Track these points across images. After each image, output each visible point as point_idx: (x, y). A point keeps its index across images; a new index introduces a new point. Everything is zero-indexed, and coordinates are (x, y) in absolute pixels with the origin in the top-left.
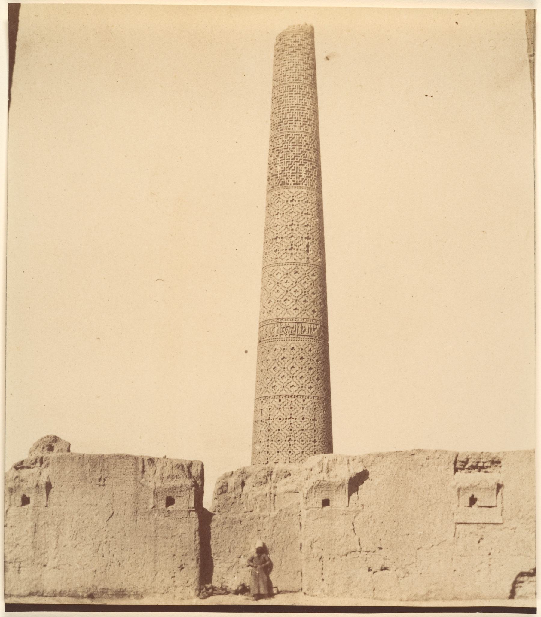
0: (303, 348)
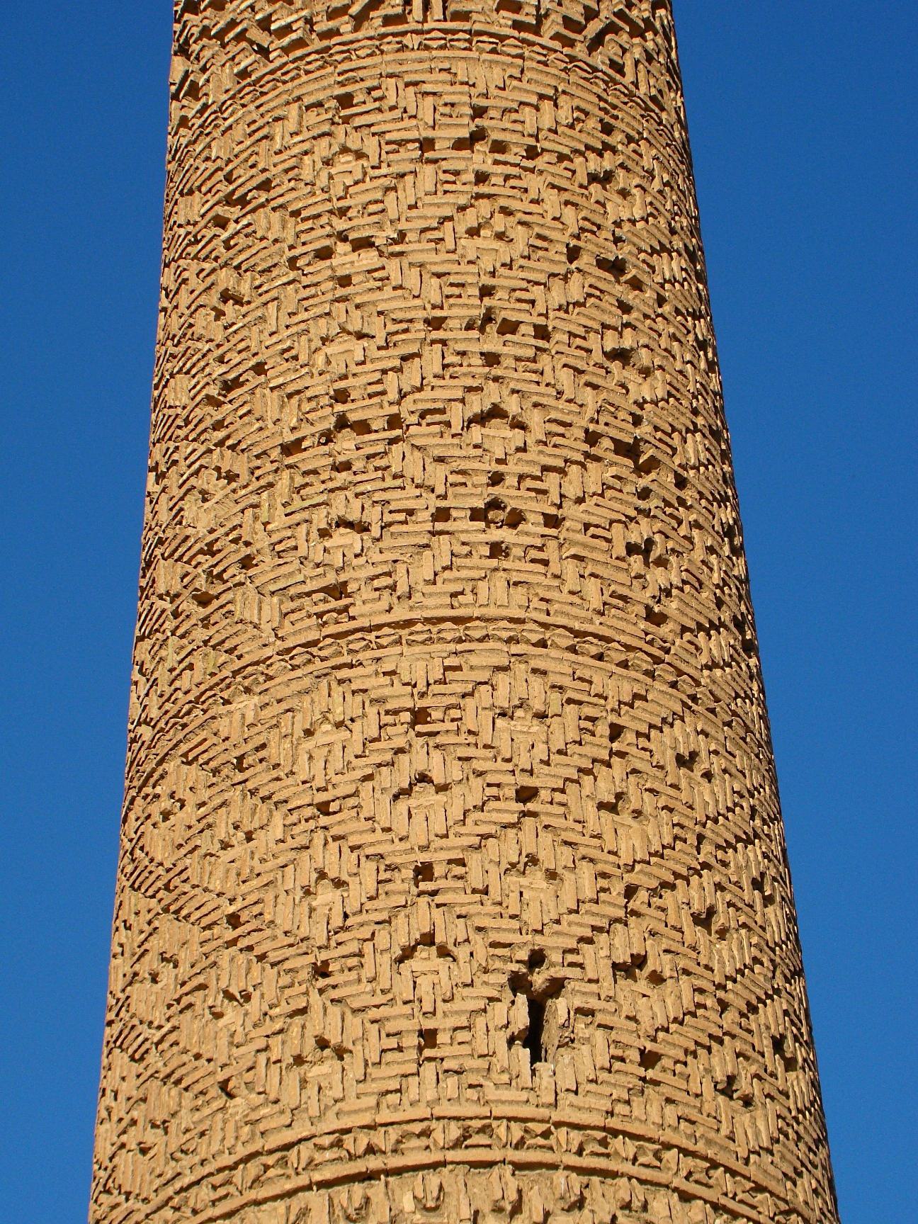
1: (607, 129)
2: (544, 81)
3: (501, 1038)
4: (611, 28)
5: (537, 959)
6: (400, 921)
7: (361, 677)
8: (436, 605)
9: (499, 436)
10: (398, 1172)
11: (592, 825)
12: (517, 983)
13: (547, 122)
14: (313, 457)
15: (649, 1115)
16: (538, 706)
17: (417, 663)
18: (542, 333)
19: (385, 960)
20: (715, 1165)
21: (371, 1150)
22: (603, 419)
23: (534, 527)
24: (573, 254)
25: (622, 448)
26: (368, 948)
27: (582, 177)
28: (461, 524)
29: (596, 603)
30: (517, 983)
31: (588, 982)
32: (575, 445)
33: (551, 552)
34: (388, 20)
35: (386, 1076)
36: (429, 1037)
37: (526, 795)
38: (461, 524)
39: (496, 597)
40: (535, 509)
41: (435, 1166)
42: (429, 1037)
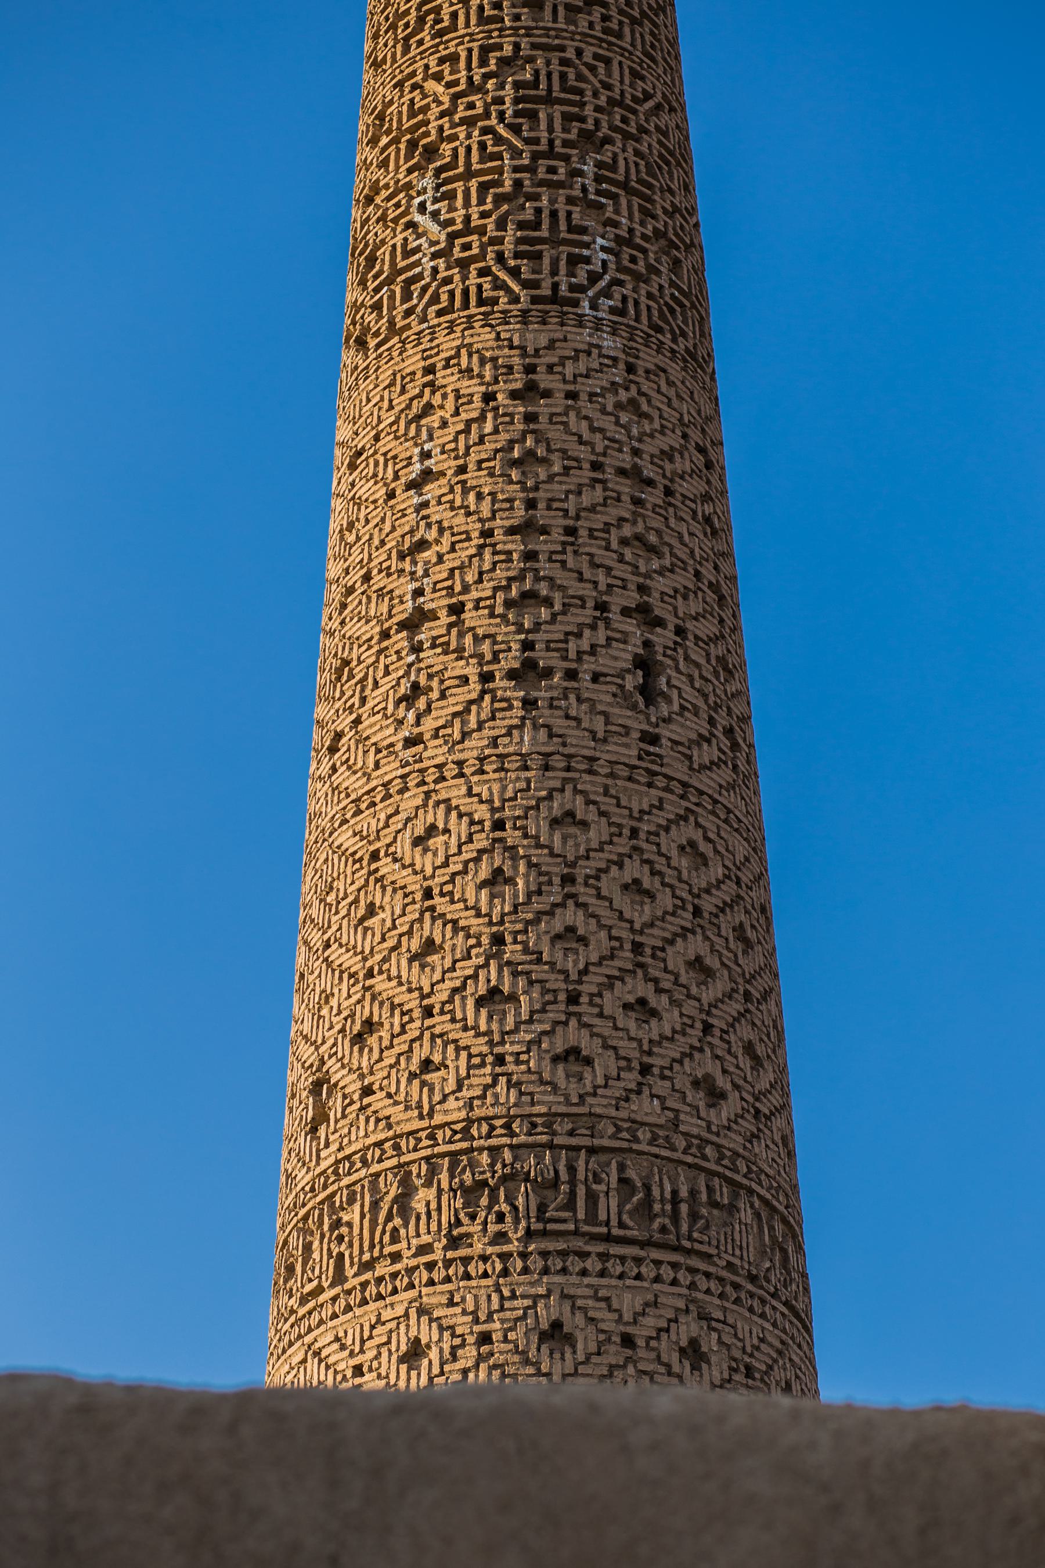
0: (639, 1334)
34: (440, 313)
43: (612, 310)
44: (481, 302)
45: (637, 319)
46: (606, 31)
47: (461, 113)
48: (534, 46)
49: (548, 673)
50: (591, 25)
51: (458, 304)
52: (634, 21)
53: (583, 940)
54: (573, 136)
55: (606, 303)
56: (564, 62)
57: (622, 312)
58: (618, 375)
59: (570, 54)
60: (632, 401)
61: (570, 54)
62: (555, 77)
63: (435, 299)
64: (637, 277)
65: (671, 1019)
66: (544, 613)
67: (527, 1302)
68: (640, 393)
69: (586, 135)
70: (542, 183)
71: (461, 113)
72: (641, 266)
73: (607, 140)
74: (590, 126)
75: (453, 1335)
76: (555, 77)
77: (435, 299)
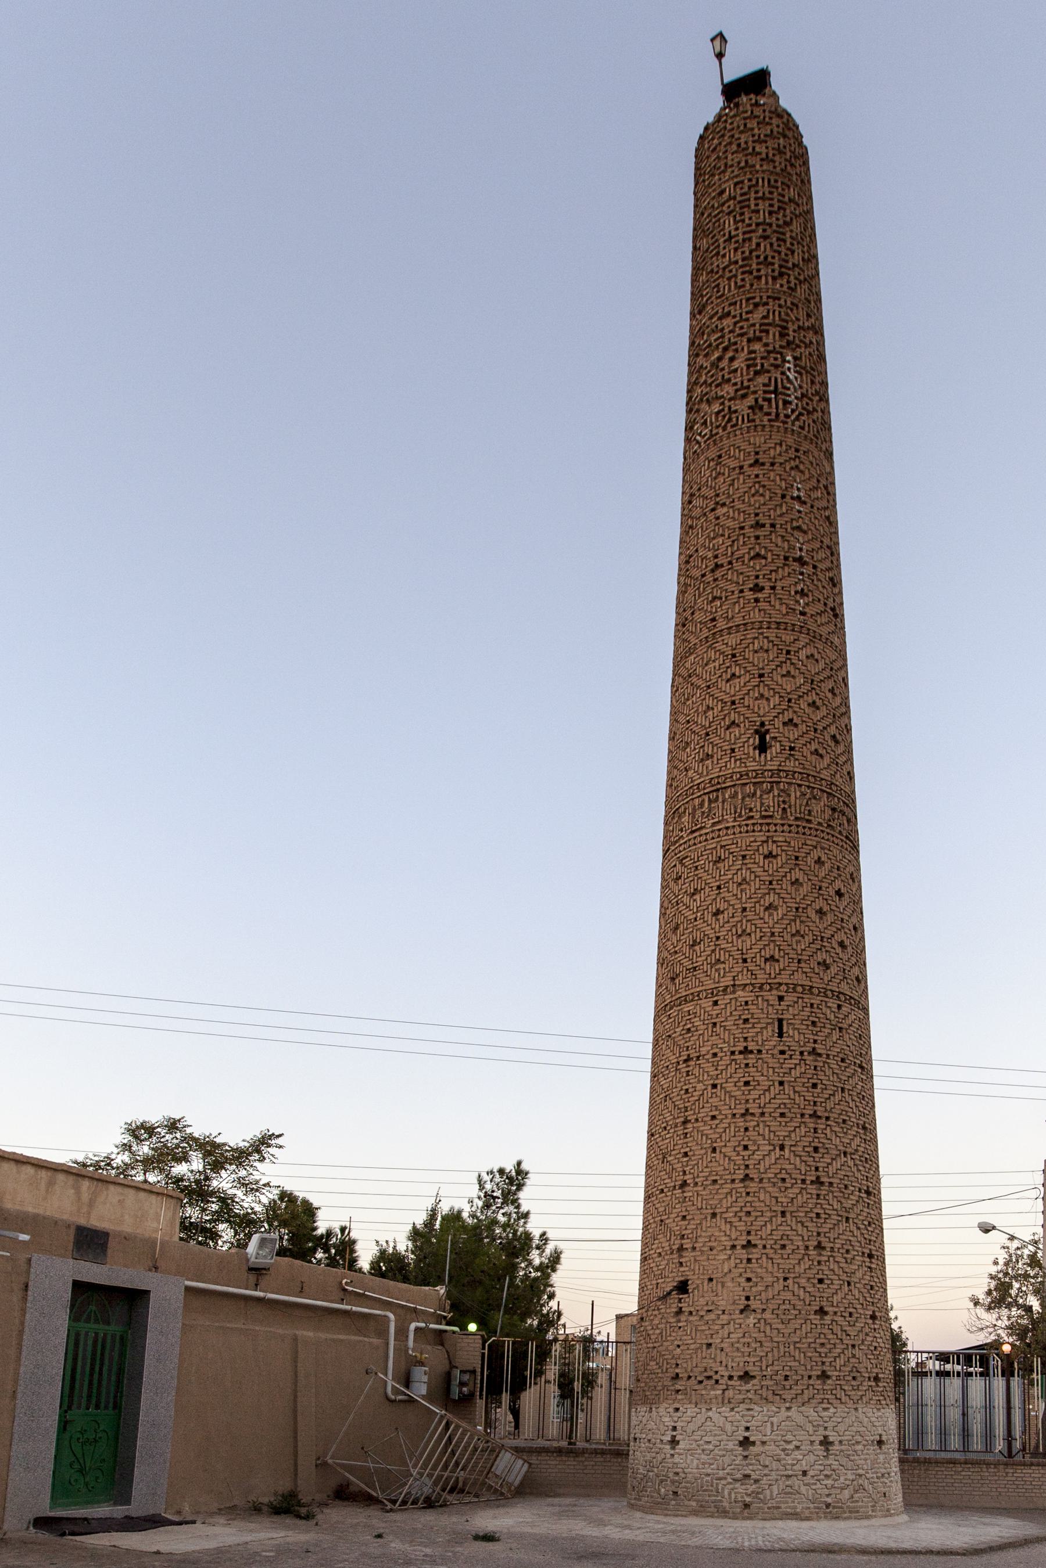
1: (797, 450)
2: (777, 437)
3: (751, 748)
4: (801, 414)
5: (762, 724)
6: (727, 719)
7: (719, 646)
8: (738, 621)
9: (758, 564)
10: (725, 788)
11: (817, 971)
12: (757, 732)
13: (778, 452)
14: (709, 578)
15: (790, 765)
16: (765, 648)
17: (733, 640)
18: (773, 526)
19: (762, 908)
20: (808, 775)
21: (718, 783)
22: (866, 1366)
23: (767, 591)
24: (783, 496)
25: (795, 560)
26: (757, 905)
27: (788, 469)
28: (747, 593)
29: (784, 612)
30: (757, 732)
31: (776, 730)
32: (780, 562)
33: (772, 599)
34: (732, 426)
35: (722, 763)
36: (733, 750)
37: (761, 676)
38: (747, 593)
39: (756, 616)
40: (767, 585)
41: (734, 786)
42: (733, 750)
43: (800, 427)
44: (749, 421)
45: (809, 432)
46: (789, 288)
47: (738, 331)
48: (768, 297)
49: (763, 588)
50: (782, 286)
51: (740, 422)
52: (800, 282)
53: (796, 725)
54: (784, 344)
55: (797, 423)
56: (780, 306)
57: (802, 428)
58: (792, 453)
59: (782, 302)
60: (797, 467)
61: (782, 302)
62: (777, 313)
63: (730, 420)
64: (809, 412)
65: (803, 728)
66: (763, 561)
67: (761, 864)
68: (801, 462)
69: (789, 343)
70: (772, 365)
71: (738, 331)
72: (810, 408)
73: (798, 346)
74: (791, 338)
75: (761, 931)
76: (777, 313)
77: (730, 420)
